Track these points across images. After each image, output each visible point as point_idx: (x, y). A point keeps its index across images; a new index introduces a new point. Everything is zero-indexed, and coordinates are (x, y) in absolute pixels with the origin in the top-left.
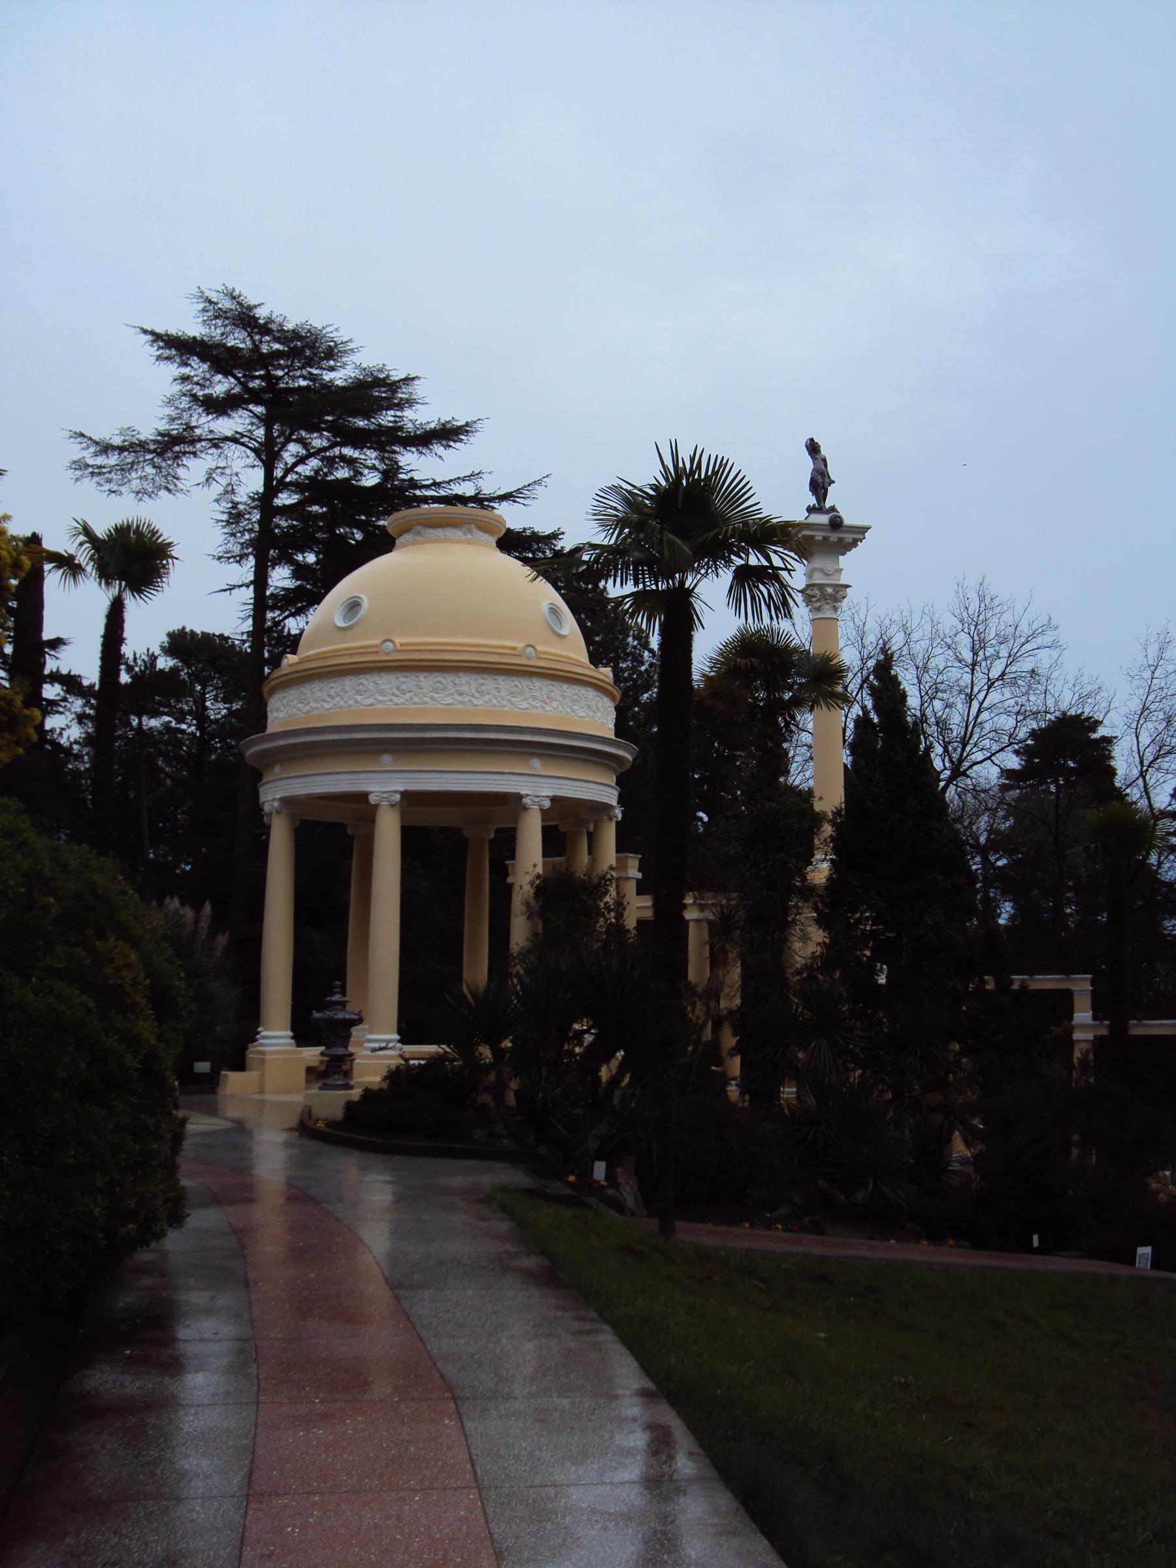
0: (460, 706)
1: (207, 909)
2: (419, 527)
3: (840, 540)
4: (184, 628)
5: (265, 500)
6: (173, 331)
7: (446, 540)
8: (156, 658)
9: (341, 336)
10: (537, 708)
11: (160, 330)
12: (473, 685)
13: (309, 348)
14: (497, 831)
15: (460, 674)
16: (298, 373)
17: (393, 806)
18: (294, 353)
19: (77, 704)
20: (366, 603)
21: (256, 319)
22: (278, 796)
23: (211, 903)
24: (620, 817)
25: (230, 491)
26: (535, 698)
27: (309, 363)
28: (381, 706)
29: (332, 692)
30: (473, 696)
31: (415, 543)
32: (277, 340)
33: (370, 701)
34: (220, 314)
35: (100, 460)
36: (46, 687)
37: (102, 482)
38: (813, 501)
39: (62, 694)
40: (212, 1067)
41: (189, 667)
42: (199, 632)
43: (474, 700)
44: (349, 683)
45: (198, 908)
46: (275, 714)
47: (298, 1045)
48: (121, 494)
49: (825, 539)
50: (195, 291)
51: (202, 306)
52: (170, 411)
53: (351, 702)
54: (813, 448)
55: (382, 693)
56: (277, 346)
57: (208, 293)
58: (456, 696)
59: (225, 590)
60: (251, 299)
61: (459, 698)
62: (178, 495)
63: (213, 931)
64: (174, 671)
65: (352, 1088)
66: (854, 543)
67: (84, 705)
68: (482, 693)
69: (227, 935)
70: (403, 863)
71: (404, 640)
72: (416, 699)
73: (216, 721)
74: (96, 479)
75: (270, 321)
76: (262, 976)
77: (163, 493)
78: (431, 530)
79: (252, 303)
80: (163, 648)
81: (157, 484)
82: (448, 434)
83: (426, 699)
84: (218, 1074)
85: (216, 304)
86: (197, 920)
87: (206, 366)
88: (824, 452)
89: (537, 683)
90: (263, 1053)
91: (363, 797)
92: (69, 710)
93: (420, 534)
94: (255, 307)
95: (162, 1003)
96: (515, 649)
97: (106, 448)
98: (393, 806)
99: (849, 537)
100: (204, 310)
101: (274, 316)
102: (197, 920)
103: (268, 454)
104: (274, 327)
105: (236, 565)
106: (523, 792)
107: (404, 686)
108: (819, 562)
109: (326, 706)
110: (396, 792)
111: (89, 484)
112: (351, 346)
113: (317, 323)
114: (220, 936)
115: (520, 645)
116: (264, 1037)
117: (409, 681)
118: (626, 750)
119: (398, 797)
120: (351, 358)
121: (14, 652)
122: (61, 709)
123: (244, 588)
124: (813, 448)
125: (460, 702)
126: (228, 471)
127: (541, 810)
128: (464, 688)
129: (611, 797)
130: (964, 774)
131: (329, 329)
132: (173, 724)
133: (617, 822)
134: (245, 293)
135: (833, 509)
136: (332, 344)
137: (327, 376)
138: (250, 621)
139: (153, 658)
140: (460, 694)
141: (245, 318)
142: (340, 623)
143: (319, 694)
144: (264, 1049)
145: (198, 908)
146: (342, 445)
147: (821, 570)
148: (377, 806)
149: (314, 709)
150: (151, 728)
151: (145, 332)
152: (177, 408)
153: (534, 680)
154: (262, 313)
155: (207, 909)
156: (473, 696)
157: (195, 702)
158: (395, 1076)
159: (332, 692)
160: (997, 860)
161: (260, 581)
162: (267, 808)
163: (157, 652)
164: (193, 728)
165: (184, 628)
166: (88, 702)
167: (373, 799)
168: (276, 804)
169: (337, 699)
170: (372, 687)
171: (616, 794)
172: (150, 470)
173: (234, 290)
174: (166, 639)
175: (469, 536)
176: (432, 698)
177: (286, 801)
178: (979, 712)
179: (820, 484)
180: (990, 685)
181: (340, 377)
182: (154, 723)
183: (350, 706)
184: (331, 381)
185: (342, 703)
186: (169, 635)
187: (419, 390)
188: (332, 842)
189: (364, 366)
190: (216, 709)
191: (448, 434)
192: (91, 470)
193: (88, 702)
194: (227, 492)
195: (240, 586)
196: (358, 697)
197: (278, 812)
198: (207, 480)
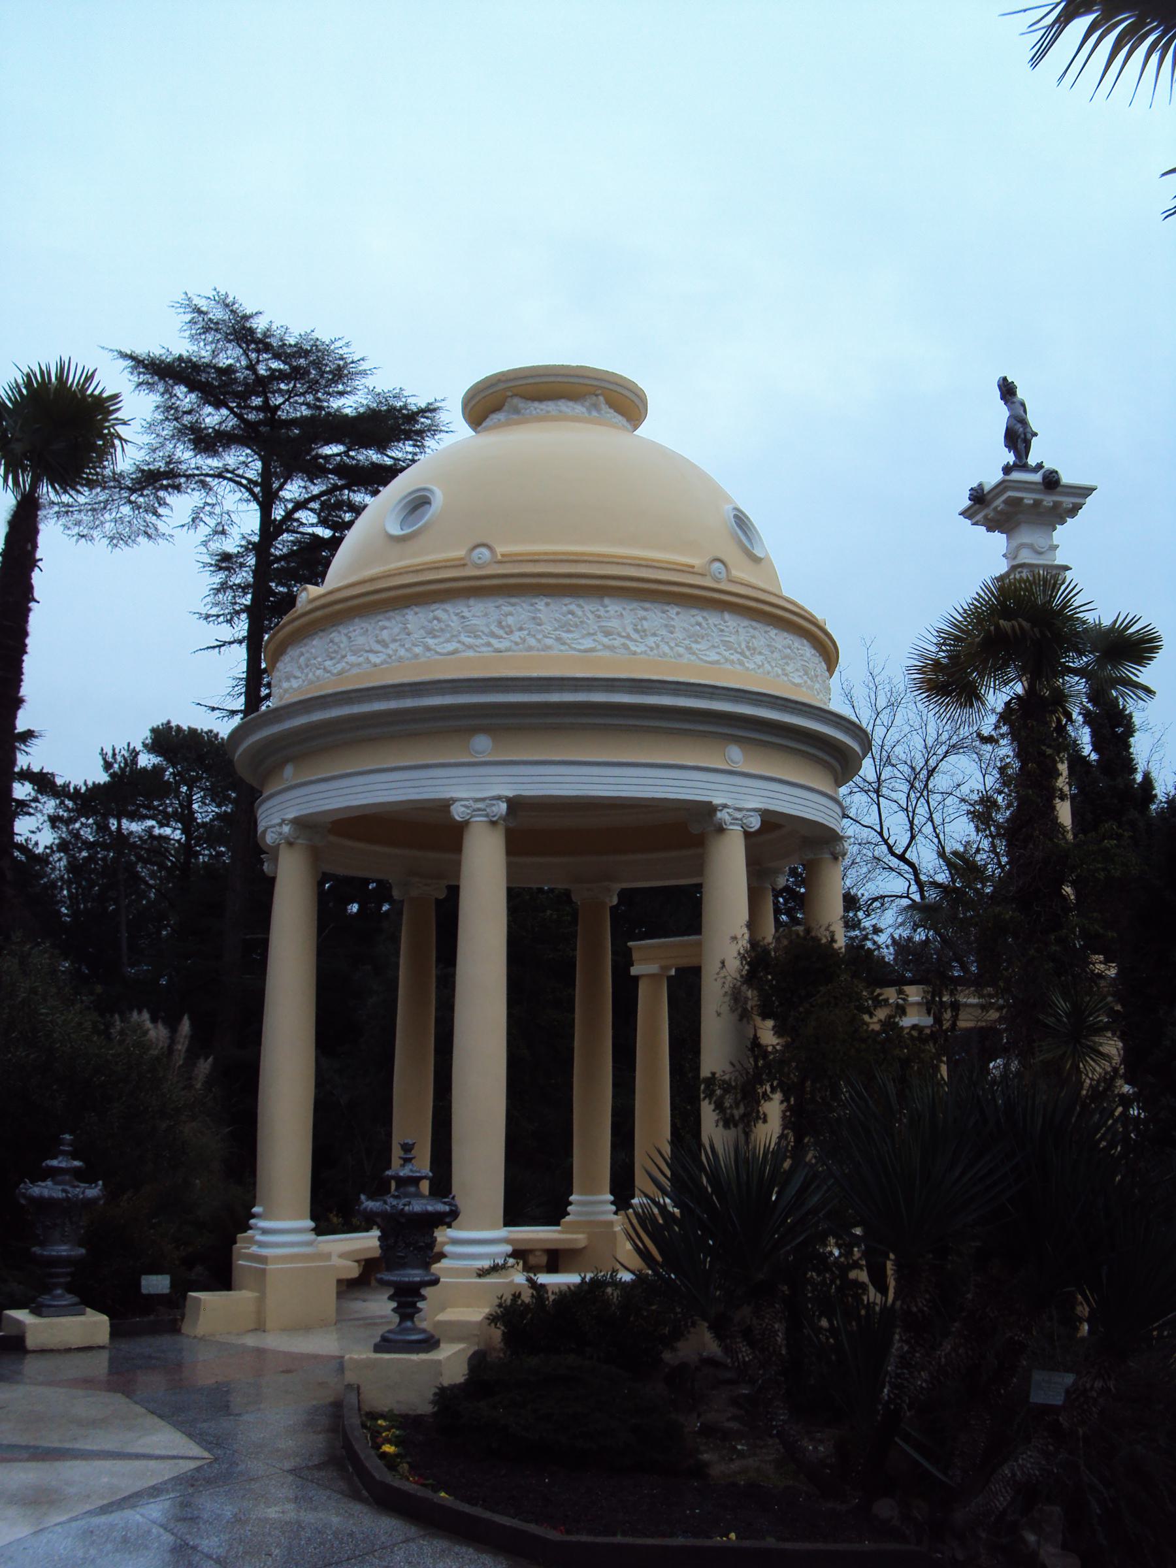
0: (607, 654)
1: (185, 1026)
2: (515, 401)
3: (1057, 505)
4: (169, 722)
5: (262, 547)
6: (157, 351)
7: (562, 418)
8: (137, 754)
9: (353, 352)
10: (732, 662)
11: (141, 351)
12: (629, 619)
13: (313, 366)
14: (624, 895)
16: (301, 400)
17: (493, 823)
18: (297, 374)
19: (50, 805)
20: (439, 499)
21: (251, 331)
22: (291, 816)
23: (190, 1019)
25: (220, 532)
26: (728, 645)
27: (313, 387)
28: (470, 654)
29: (385, 635)
30: (628, 637)
31: (508, 424)
32: (276, 357)
33: (450, 647)
34: (210, 327)
36: (16, 786)
37: (70, 525)
38: (1010, 458)
39: (33, 794)
40: (173, 1285)
41: (174, 767)
42: (185, 728)
44: (416, 619)
45: (173, 1028)
46: (285, 685)
47: (319, 1231)
48: (92, 539)
49: (1037, 503)
50: (180, 297)
51: (188, 317)
53: (417, 650)
54: (1007, 390)
55: (473, 632)
56: (275, 365)
57: (197, 301)
58: (600, 637)
59: (214, 647)
61: (605, 640)
62: (160, 541)
63: (192, 1056)
64: (157, 770)
65: (429, 1343)
66: (1074, 511)
67: (57, 807)
68: (643, 633)
69: (210, 1059)
71: (516, 546)
72: (532, 642)
73: (204, 825)
74: (63, 520)
75: (267, 334)
76: (259, 1111)
77: (142, 539)
78: (536, 404)
79: (248, 312)
80: (145, 745)
81: (135, 528)
83: (549, 642)
84: (185, 1297)
85: (206, 313)
86: (172, 1040)
87: (193, 396)
88: (1021, 394)
89: (731, 622)
90: (263, 1259)
92: (41, 811)
93: (517, 411)
94: (251, 316)
96: (693, 567)
98: (493, 823)
100: (192, 322)
101: (274, 327)
102: (172, 1040)
103: (266, 499)
104: (275, 342)
105: (226, 626)
106: (717, 801)
108: (1026, 536)
109: (374, 659)
110: (499, 798)
112: (364, 366)
113: (324, 335)
114: (202, 1061)
116: (265, 1232)
117: (518, 612)
119: (503, 807)
120: (363, 380)
121: (10, 790)
122: (32, 811)
123: (236, 645)
124: (1007, 390)
125: (606, 647)
126: (217, 510)
127: (747, 835)
128: (614, 624)
131: (338, 344)
132: (157, 831)
134: (241, 299)
135: (1040, 466)
136: (341, 363)
137: (335, 403)
138: (243, 698)
139: (135, 754)
140: (607, 634)
141: (241, 332)
142: (395, 530)
143: (361, 640)
144: (264, 1252)
145: (173, 1028)
146: (348, 486)
147: (1031, 547)
149: (352, 665)
150: (131, 833)
152: (158, 435)
153: (727, 616)
154: (259, 325)
155: (185, 1026)
156: (628, 637)
157: (181, 805)
158: (513, 1317)
159: (385, 635)
162: (270, 838)
163: (139, 747)
164: (178, 832)
165: (169, 722)
166: (62, 802)
168: (286, 829)
169: (393, 646)
170: (455, 623)
172: (126, 510)
173: (227, 295)
174: (148, 734)
175: (594, 414)
176: (558, 639)
177: (302, 824)
179: (1018, 437)
181: (348, 404)
182: (135, 827)
183: (416, 656)
184: (339, 409)
185: (402, 652)
186: (153, 730)
189: (378, 390)
190: (204, 811)
192: (56, 509)
193: (62, 802)
194: (216, 532)
195: (230, 643)
196: (431, 642)
197: (290, 844)
198: (193, 520)
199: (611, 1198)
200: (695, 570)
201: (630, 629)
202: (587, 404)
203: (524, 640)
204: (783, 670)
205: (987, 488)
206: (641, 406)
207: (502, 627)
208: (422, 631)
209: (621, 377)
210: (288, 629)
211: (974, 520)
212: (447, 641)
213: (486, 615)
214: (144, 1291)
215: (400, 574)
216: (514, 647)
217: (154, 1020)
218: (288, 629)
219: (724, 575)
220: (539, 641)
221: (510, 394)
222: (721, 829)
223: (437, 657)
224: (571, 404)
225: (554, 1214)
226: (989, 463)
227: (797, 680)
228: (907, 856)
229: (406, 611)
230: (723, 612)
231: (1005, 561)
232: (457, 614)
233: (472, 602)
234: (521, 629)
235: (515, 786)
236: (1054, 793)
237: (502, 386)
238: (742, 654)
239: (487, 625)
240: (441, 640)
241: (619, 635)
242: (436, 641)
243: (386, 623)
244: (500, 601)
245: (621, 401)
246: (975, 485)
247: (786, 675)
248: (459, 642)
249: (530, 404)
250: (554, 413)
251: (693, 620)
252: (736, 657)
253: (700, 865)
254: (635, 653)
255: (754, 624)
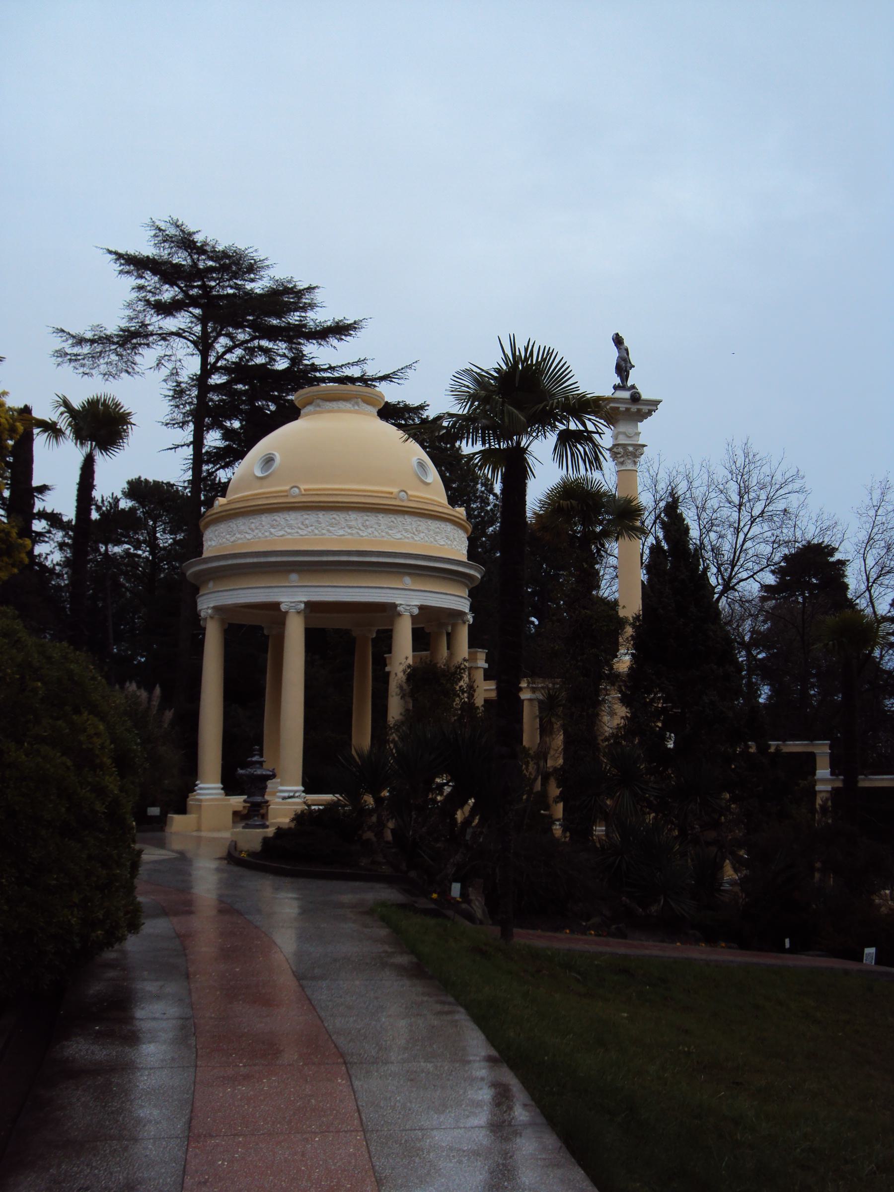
0: (350, 537)
1: (158, 691)
2: (318, 401)
3: (639, 410)
4: (140, 477)
5: (201, 380)
6: (131, 252)
7: (339, 411)
8: (119, 500)
9: (259, 255)
10: (408, 538)
11: (122, 251)
12: (360, 521)
13: (235, 264)
14: (378, 632)
15: (350, 513)
16: (227, 284)
17: (299, 613)
18: (224, 269)
19: (59, 535)
20: (278, 458)
21: (195, 243)
22: (212, 605)
23: (161, 687)
24: (471, 621)
25: (175, 373)
26: (406, 531)
27: (235, 276)
28: (289, 537)
29: (253, 526)
30: (360, 529)
31: (315, 413)
32: (211, 258)
33: (281, 533)
34: (167, 239)
35: (76, 350)
36: (35, 522)
37: (78, 366)
38: (618, 381)
39: (47, 527)
40: (161, 811)
41: (144, 507)
42: (151, 480)
43: (360, 532)
44: (265, 519)
45: (150, 691)
46: (209, 543)
47: (227, 795)
48: (92, 375)
49: (628, 410)
50: (148, 221)
51: (153, 232)
52: (129, 312)
53: (267, 534)
54: (618, 341)
55: (291, 527)
56: (210, 263)
57: (158, 223)
58: (347, 529)
59: (171, 449)
60: (191, 227)
61: (349, 531)
62: (136, 376)
63: (162, 708)
64: (132, 510)
65: (267, 827)
66: (650, 413)
67: (64, 536)
68: (367, 527)
69: (172, 710)
70: (306, 656)
71: (307, 487)
72: (316, 532)
73: (165, 548)
74: (73, 364)
75: (205, 244)
76: (199, 742)
77: (124, 375)
78: (328, 403)
79: (192, 230)
80: (124, 493)
81: (119, 368)
82: (340, 330)
83: (324, 532)
84: (166, 816)
85: (164, 231)
86: (150, 700)
87: (156, 279)
88: (626, 343)
89: (408, 519)
90: (200, 800)
91: (276, 606)
92: (53, 540)
93: (319, 406)
94: (194, 233)
95: (123, 763)
96: (392, 493)
97: (80, 341)
98: (299, 613)
99: (645, 409)
100: (155, 236)
101: (208, 240)
102: (150, 700)
103: (204, 345)
104: (208, 248)
105: (180, 430)
106: (397, 602)
107: (307, 522)
108: (622, 427)
109: (248, 537)
110: (301, 602)
111: (68, 368)
112: (267, 263)
113: (241, 246)
114: (167, 712)
115: (395, 490)
116: (201, 789)
117: (311, 518)
118: (476, 570)
119: (303, 606)
120: (267, 272)
121: (11, 495)
122: (47, 539)
123: (185, 447)
124: (618, 341)
125: (350, 534)
126: (173, 358)
127: (412, 616)
128: (353, 523)
129: (464, 606)
130: (733, 588)
131: (250, 250)
132: (132, 551)
133: (469, 625)
134: (186, 223)
135: (633, 387)
136: (252, 261)
137: (249, 286)
138: (190, 472)
139: (117, 500)
140: (350, 528)
141: (186, 242)
142: (259, 474)
143: (242, 528)
144: (201, 797)
145: (150, 691)
146: (260, 338)
147: (624, 433)
148: (287, 613)
149: (239, 539)
150: (115, 554)
151: (110, 252)
152: (134, 310)
153: (406, 517)
154: (199, 238)
155: (158, 691)
156: (360, 529)
157: (148, 534)
158: (300, 818)
159: (253, 526)
160: (758, 653)
161: (198, 442)
162: (203, 614)
163: (120, 495)
164: (147, 554)
165: (140, 477)
166: (67, 533)
167: (283, 608)
168: (210, 611)
169: (257, 531)
170: (283, 522)
171: (469, 603)
172: (114, 357)
173: (178, 220)
174: (126, 486)
175: (356, 408)
176: (328, 530)
177: (218, 609)
178: (744, 541)
179: (623, 368)
180: (753, 521)
181: (258, 286)
182: (117, 550)
183: (266, 537)
184: (252, 290)
185: (260, 535)
186: (129, 483)
187: (318, 296)
188: (252, 640)
189: (277, 278)
190: (165, 539)
191: (340, 330)
192: (69, 357)
193: (67, 533)
194: (172, 374)
195: (182, 446)
196: (272, 530)
197: (212, 618)
198: (158, 365)
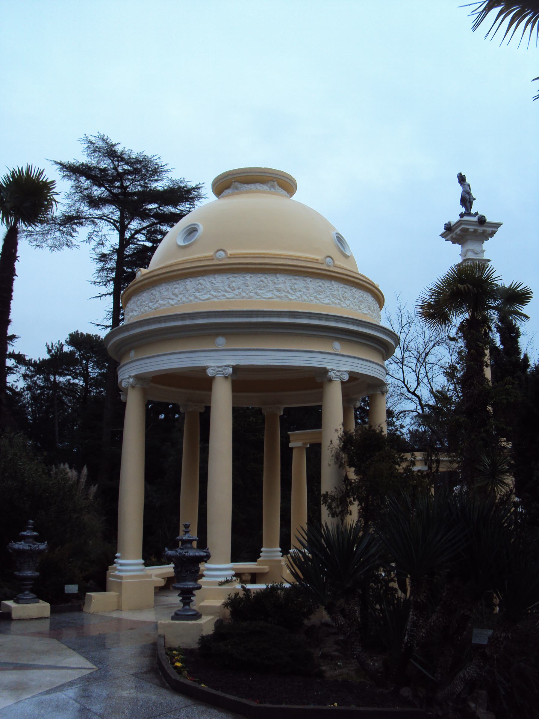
0: (278, 300)
1: (85, 471)
2: (236, 184)
3: (484, 232)
4: (77, 331)
5: (120, 251)
6: (72, 161)
7: (258, 191)
8: (63, 346)
9: (162, 162)
10: (336, 304)
11: (65, 161)
12: (288, 284)
13: (144, 168)
14: (286, 410)
16: (138, 183)
17: (226, 378)
18: (136, 171)
19: (23, 369)
20: (201, 229)
21: (115, 152)
22: (133, 374)
23: (87, 467)
25: (101, 244)
26: (334, 296)
27: (143, 177)
28: (216, 300)
29: (176, 291)
30: (288, 292)
31: (233, 194)
32: (127, 163)
33: (206, 297)
34: (96, 150)
36: (8, 360)
37: (32, 241)
38: (463, 210)
39: (15, 364)
40: (79, 589)
41: (80, 352)
42: (85, 334)
44: (190, 284)
45: (79, 471)
46: (131, 314)
47: (146, 564)
48: (42, 247)
49: (475, 231)
50: (83, 136)
51: (86, 145)
53: (191, 298)
54: (462, 179)
55: (217, 290)
56: (126, 167)
57: (90, 138)
58: (275, 292)
59: (98, 297)
61: (277, 294)
62: (73, 248)
63: (88, 484)
64: (72, 353)
65: (197, 616)
66: (492, 234)
67: (26, 370)
68: (295, 290)
69: (96, 486)
72: (244, 294)
73: (93, 378)
74: (29, 239)
75: (122, 153)
76: (119, 509)
77: (65, 247)
78: (246, 185)
79: (114, 143)
80: (66, 342)
81: (62, 242)
83: (252, 294)
84: (85, 595)
85: (94, 144)
86: (79, 477)
87: (88, 182)
88: (468, 181)
89: (335, 285)
90: (120, 577)
92: (19, 372)
93: (237, 188)
94: (115, 145)
96: (318, 260)
98: (226, 378)
100: (88, 148)
101: (126, 150)
102: (79, 477)
103: (122, 229)
104: (126, 157)
105: (104, 287)
106: (328, 367)
108: (470, 246)
109: (171, 302)
110: (229, 366)
112: (167, 168)
113: (148, 154)
114: (92, 486)
116: (121, 565)
117: (237, 280)
119: (231, 370)
120: (167, 174)
121: (4, 362)
122: (15, 372)
123: (108, 296)
124: (462, 179)
125: (278, 297)
126: (100, 234)
127: (342, 383)
128: (281, 286)
131: (155, 158)
132: (72, 381)
134: (110, 137)
135: (477, 214)
136: (156, 166)
137: (154, 185)
138: (111, 320)
139: (62, 346)
140: (278, 291)
141: (110, 152)
142: (181, 243)
143: (165, 294)
144: (121, 574)
145: (79, 471)
146: (160, 223)
147: (472, 251)
149: (161, 305)
150: (60, 382)
152: (72, 200)
153: (333, 282)
154: (119, 149)
155: (85, 471)
156: (288, 292)
157: (83, 369)
158: (235, 604)
159: (176, 291)
162: (124, 384)
163: (64, 343)
164: (82, 381)
165: (77, 331)
166: (28, 368)
168: (131, 380)
169: (180, 296)
170: (208, 286)
172: (58, 234)
173: (104, 135)
174: (68, 337)
175: (272, 190)
176: (256, 293)
177: (138, 378)
179: (467, 200)
181: (160, 185)
182: (62, 379)
183: (191, 301)
184: (155, 188)
185: (184, 299)
186: (70, 335)
189: (173, 179)
190: (94, 372)
192: (26, 233)
193: (28, 368)
194: (99, 244)
195: (106, 295)
196: (197, 294)
197: (133, 387)
198: (89, 239)
199: (280, 549)
200: (319, 261)
201: (289, 289)
202: (269, 185)
203: (240, 294)
204: (359, 307)
205: (452, 224)
206: (294, 186)
207: (230, 288)
208: (193, 290)
209: (285, 173)
210: (132, 288)
211: (447, 239)
212: (205, 294)
213: (223, 282)
214: (66, 592)
215: (184, 263)
216: (236, 297)
217: (71, 468)
218: (132, 288)
219: (332, 263)
220: (247, 294)
221: (234, 181)
222: (330, 380)
223: (200, 301)
224: (262, 185)
225: (254, 557)
226: (453, 213)
227: (365, 312)
228: (416, 392)
229: (186, 280)
230: (331, 280)
231: (461, 257)
232: (209, 282)
233: (216, 276)
234: (239, 288)
235: (236, 361)
236: (483, 363)
237: (230, 177)
238: (340, 300)
239: (223, 287)
240: (202, 293)
241: (284, 291)
242: (200, 294)
243: (177, 286)
244: (229, 276)
245: (285, 184)
246: (447, 222)
247: (360, 309)
248: (210, 294)
249: (243, 185)
250: (254, 189)
251: (317, 284)
252: (337, 301)
253: (321, 396)
254: (291, 300)
255: (346, 286)
